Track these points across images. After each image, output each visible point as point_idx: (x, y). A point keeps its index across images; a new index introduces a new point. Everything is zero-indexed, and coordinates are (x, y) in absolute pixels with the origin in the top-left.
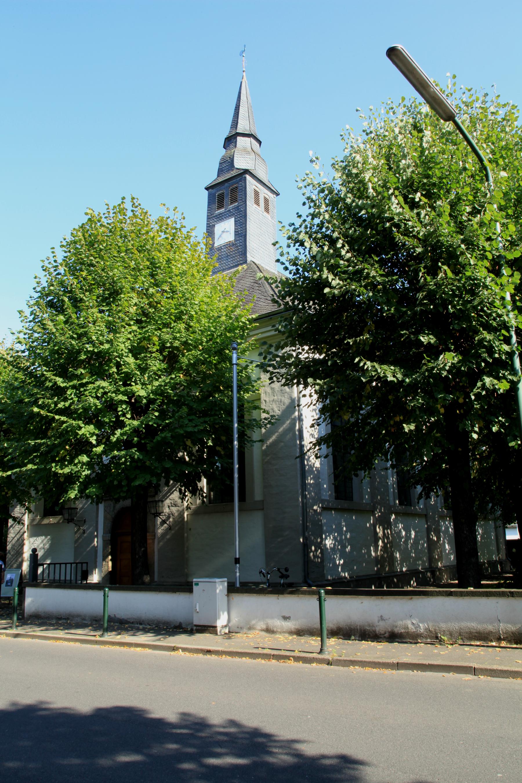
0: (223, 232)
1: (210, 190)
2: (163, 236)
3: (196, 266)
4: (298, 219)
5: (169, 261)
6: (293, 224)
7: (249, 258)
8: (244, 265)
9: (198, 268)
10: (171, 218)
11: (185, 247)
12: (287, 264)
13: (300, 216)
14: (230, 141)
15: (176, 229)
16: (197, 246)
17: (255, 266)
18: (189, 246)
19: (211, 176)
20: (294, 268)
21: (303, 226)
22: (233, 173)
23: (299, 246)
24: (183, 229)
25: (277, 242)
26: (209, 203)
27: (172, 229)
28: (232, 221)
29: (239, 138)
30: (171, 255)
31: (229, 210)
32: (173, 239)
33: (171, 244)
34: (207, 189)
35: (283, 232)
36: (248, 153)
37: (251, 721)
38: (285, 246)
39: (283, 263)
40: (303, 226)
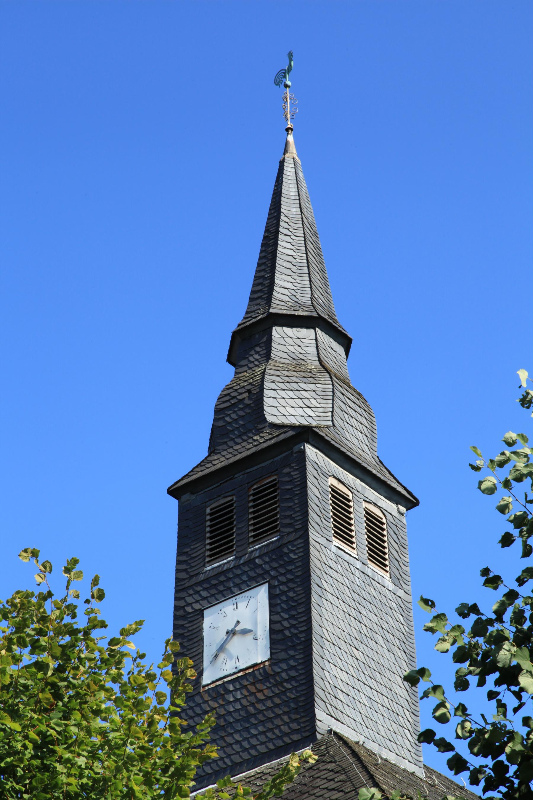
0: (231, 633)
1: (186, 497)
2: (27, 658)
3: (142, 759)
4: (489, 590)
5: (44, 746)
6: (475, 609)
7: (324, 721)
8: (307, 751)
9: (148, 766)
10: (57, 597)
11: (102, 695)
12: (462, 748)
13: (493, 581)
14: (250, 342)
15: (73, 632)
16: (142, 689)
17: (344, 750)
18: (116, 688)
19: (189, 449)
20: (489, 762)
21: (508, 615)
22: (263, 440)
23: (498, 683)
24: (95, 634)
25: (422, 672)
26: (180, 537)
27: (59, 632)
28: (261, 596)
29: (277, 332)
30: (53, 726)
31: (251, 561)
32: (60, 669)
33: (54, 685)
34: (173, 492)
35: (439, 635)
36: (309, 375)
37: (77, 614)
38: (448, 682)
39: (445, 746)
40: (508, 615)
